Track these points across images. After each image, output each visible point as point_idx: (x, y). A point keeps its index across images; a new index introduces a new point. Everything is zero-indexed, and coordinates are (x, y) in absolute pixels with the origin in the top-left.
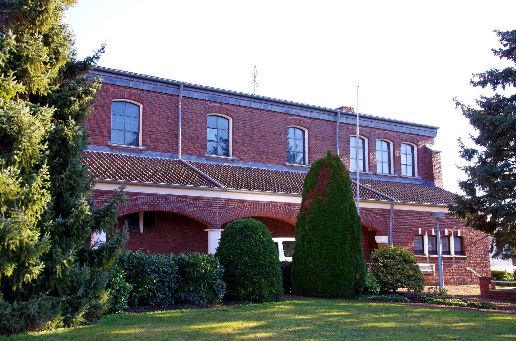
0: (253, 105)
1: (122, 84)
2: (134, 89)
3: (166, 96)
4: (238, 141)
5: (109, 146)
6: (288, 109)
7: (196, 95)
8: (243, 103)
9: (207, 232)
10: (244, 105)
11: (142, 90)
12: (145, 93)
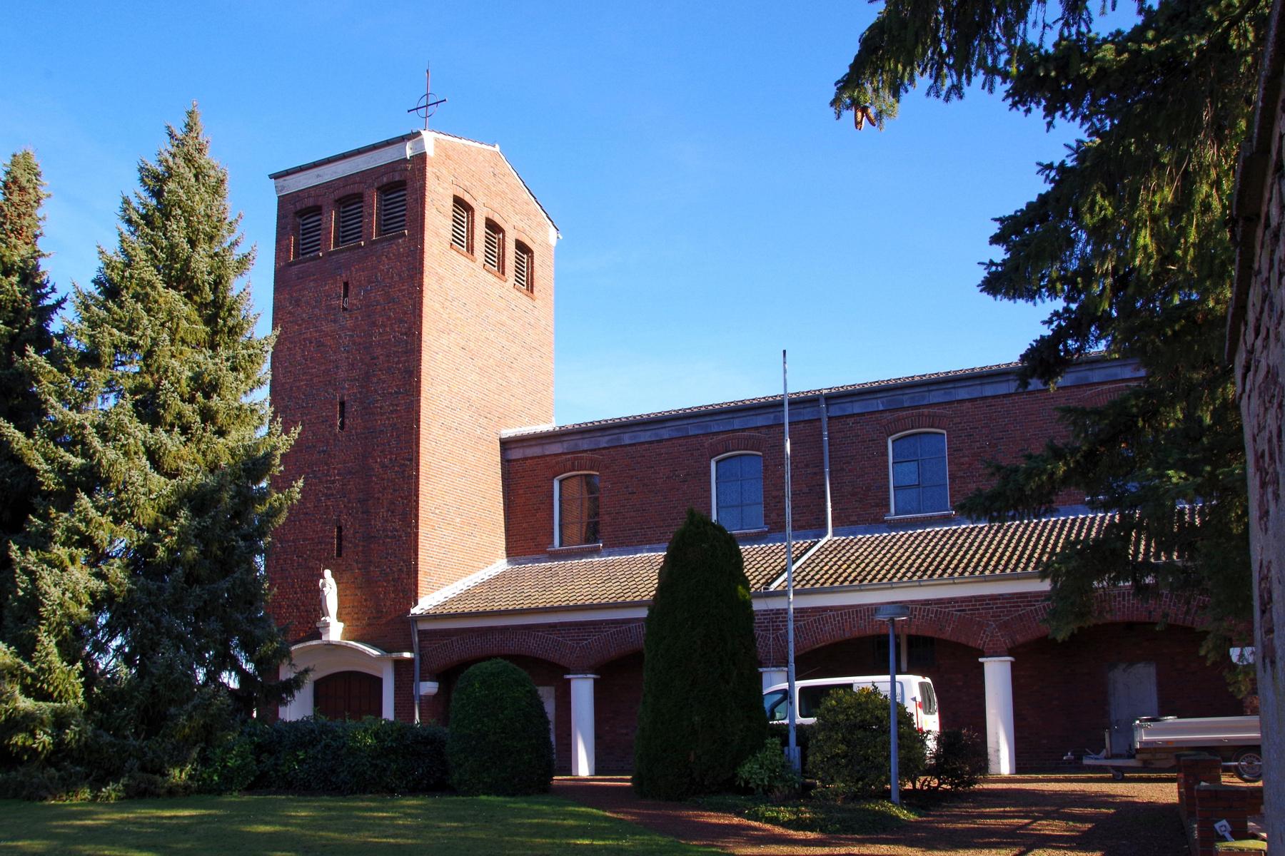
0: (989, 391)
1: (722, 429)
2: (744, 430)
3: (801, 426)
4: (961, 474)
5: (885, 521)
6: (1079, 374)
7: (857, 408)
8: (963, 394)
9: (569, 680)
10: (765, 423)
11: (757, 428)
12: (968, 404)
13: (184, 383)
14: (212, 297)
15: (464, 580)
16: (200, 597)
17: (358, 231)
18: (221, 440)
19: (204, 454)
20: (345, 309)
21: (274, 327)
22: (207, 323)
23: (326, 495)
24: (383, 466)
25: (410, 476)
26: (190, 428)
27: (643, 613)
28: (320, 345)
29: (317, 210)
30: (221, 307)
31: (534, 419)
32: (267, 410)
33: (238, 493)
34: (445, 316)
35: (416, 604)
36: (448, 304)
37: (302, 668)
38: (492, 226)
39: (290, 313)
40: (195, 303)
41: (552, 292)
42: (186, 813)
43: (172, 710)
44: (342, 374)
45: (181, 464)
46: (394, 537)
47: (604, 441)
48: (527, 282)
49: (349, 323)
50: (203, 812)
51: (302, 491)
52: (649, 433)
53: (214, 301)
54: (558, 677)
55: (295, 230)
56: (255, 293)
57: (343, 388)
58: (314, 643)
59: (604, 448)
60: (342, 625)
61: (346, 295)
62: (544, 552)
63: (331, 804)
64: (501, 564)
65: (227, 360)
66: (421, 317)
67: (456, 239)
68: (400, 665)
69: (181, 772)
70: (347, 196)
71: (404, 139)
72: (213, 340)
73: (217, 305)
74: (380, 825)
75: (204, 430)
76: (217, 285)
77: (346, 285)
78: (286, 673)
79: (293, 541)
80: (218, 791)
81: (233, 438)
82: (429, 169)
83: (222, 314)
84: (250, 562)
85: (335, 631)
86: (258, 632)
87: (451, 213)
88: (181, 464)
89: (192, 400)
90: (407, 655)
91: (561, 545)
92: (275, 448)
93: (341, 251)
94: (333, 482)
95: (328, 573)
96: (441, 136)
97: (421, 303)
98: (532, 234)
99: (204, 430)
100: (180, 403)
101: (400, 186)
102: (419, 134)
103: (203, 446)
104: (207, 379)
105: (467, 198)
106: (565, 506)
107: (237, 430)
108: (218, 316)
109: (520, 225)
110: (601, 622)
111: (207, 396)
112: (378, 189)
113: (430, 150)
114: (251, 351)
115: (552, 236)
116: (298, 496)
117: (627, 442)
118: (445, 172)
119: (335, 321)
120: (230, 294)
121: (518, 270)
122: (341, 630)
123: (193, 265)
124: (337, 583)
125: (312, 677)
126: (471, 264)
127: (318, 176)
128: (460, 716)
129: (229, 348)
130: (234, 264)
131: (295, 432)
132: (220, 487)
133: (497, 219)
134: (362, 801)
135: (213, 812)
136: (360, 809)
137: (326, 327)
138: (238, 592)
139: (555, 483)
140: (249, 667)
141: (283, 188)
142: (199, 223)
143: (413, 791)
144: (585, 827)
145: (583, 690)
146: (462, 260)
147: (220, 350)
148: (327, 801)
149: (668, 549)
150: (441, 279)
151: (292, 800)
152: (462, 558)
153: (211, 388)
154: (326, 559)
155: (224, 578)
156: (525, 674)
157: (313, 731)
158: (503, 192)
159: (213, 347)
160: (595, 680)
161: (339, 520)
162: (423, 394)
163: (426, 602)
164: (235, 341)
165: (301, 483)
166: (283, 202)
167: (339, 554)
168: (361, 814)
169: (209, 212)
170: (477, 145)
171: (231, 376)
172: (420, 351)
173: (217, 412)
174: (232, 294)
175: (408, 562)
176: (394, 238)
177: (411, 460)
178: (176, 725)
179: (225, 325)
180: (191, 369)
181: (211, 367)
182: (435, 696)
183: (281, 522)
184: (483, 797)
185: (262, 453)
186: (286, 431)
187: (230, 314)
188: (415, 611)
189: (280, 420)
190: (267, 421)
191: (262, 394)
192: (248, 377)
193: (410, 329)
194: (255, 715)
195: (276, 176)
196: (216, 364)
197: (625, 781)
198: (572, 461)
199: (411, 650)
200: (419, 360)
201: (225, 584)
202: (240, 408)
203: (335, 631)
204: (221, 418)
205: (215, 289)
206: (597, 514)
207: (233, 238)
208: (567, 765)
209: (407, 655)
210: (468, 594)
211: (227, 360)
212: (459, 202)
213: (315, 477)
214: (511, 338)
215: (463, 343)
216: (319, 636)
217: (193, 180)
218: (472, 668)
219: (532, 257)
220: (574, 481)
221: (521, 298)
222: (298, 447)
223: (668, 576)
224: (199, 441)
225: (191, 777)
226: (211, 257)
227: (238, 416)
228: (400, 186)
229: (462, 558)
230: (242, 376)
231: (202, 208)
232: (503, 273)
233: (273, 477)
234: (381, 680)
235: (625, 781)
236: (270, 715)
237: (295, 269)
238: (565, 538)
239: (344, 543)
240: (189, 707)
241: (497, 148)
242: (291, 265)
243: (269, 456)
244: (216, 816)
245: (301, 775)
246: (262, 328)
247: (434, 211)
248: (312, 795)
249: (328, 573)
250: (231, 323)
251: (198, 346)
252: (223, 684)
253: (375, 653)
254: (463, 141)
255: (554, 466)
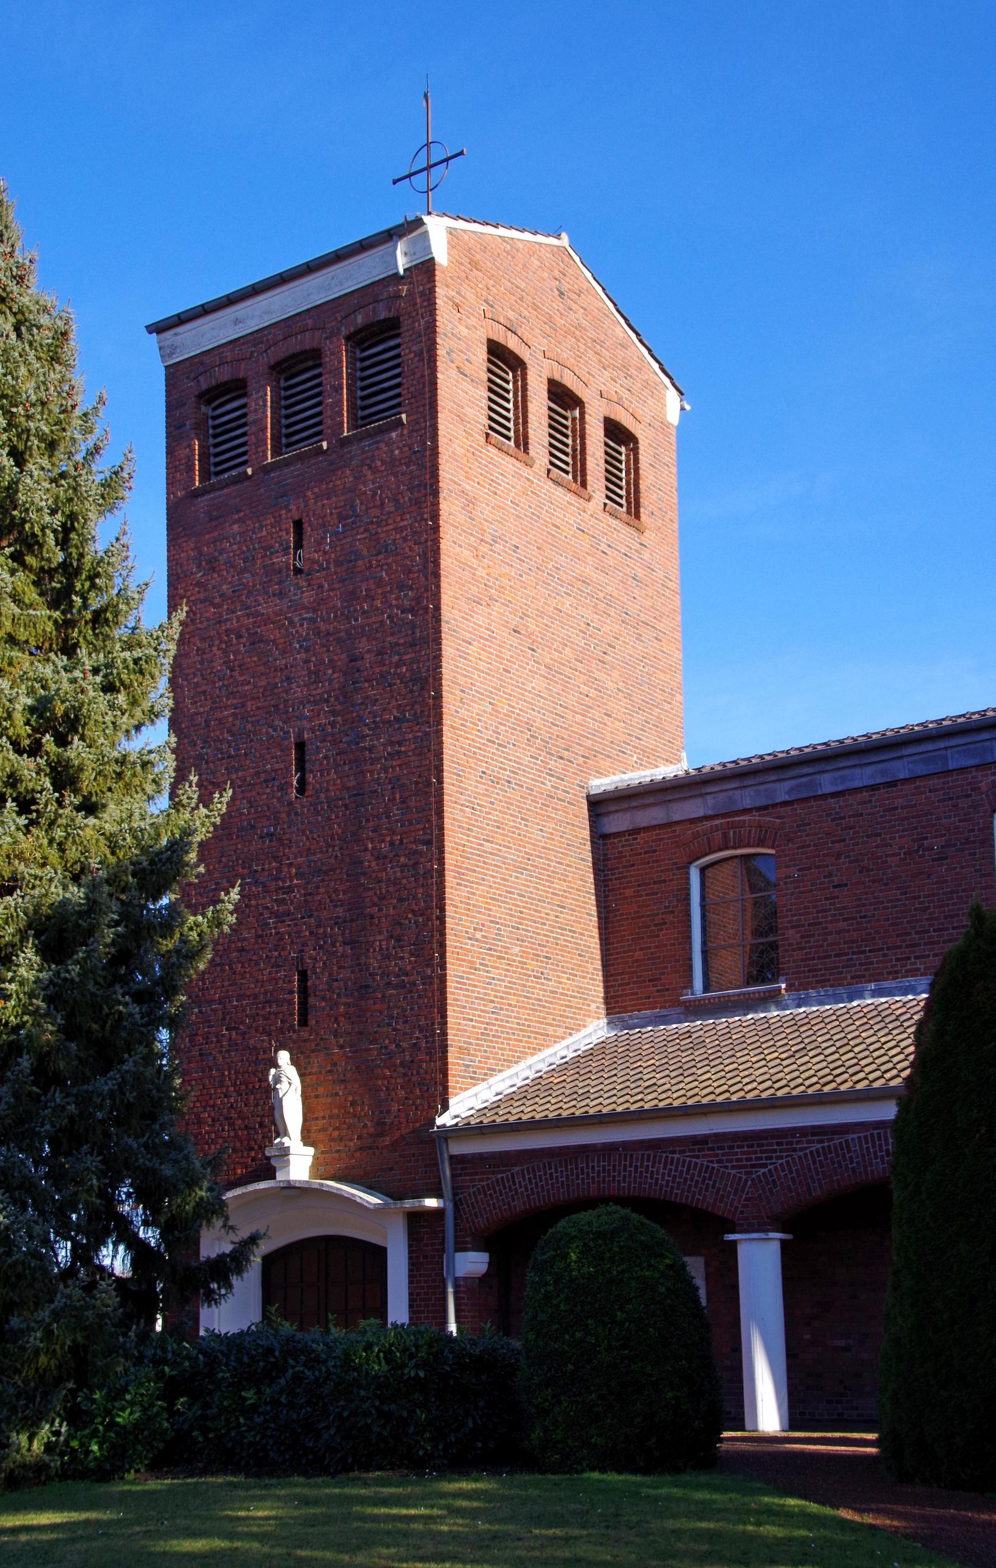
9: (734, 1243)
13: (19, 718)
14: (60, 557)
15: (531, 1060)
16: (63, 1108)
17: (317, 415)
18: (91, 821)
19: (62, 848)
20: (298, 571)
21: (173, 607)
22: (53, 605)
23: (276, 915)
24: (379, 857)
25: (428, 873)
26: (34, 801)
27: (888, 1111)
28: (256, 640)
29: (238, 387)
30: (78, 572)
31: (649, 757)
32: (166, 766)
33: (125, 917)
34: (481, 572)
35: (446, 1107)
36: (484, 549)
37: (244, 1234)
38: (561, 396)
39: (199, 584)
40: (31, 569)
41: (673, 515)
42: (45, 1518)
43: (15, 1322)
44: (298, 692)
45: (21, 867)
46: (402, 985)
47: (782, 791)
48: (627, 498)
49: (308, 597)
50: (75, 1516)
51: (237, 909)
52: (869, 770)
53: (64, 565)
54: (710, 1233)
55: (200, 427)
56: (135, 542)
57: (301, 718)
58: (262, 1185)
59: (785, 803)
60: (311, 1151)
61: (299, 545)
62: (676, 1003)
63: (306, 1491)
64: (596, 1029)
65: (96, 671)
66: (437, 576)
67: (496, 426)
68: (417, 1219)
69: (31, 1439)
70: (292, 359)
71: (391, 235)
72: (66, 640)
73: (69, 570)
74: (406, 1534)
75: (60, 803)
76: (65, 536)
77: (298, 525)
78: (214, 1244)
79: (220, 1001)
80: (105, 1472)
81: (110, 818)
82: (441, 292)
83: (78, 587)
84: (149, 1040)
85: (300, 1164)
86: (167, 1170)
87: (485, 376)
88: (21, 867)
89: (35, 750)
90: (431, 1203)
91: (706, 988)
92: (187, 832)
93: (287, 463)
94: (290, 890)
95: (284, 1057)
96: (461, 224)
97: (437, 551)
98: (635, 405)
99: (60, 803)
100: (12, 756)
101: (390, 327)
102: (419, 223)
103: (59, 834)
104: (60, 709)
105: (512, 343)
106: (712, 917)
107: (119, 803)
108: (71, 589)
109: (613, 389)
110: (793, 1131)
111: (62, 741)
112: (348, 338)
113: (440, 252)
114: (137, 653)
115: (672, 405)
116: (232, 919)
117: (828, 788)
118: (470, 296)
119: (281, 594)
120: (90, 548)
121: (611, 478)
122: (309, 1161)
123: (21, 497)
124: (301, 1075)
125: (265, 1247)
126: (525, 471)
127: (237, 322)
128: (542, 1317)
129: (96, 650)
130: (95, 490)
131: (222, 800)
132: (93, 906)
133: (569, 381)
134: (366, 1484)
135: (93, 1515)
136: (363, 1501)
137: (266, 607)
138: (131, 1097)
139: (704, 873)
140: (150, 1235)
141: (174, 349)
142: (29, 417)
143: (460, 1464)
144: (804, 1541)
145: (760, 1263)
146: (509, 464)
147: (82, 653)
148: (300, 1486)
149: (932, 988)
150: (470, 502)
151: (235, 1486)
152: (527, 1020)
153: (68, 726)
154: (281, 1031)
155: (104, 1072)
156: (661, 1233)
157: (270, 1351)
158: (579, 327)
159: (69, 649)
160: (784, 1244)
161: (301, 960)
162: (447, 720)
163: (462, 1105)
164: (107, 637)
165: (235, 894)
166: (174, 375)
167: (304, 1022)
168: (369, 1510)
169: (43, 395)
170: (527, 236)
171: (103, 700)
172: (438, 641)
173: (81, 769)
174: (97, 548)
175: (428, 1031)
176: (380, 431)
177: (428, 843)
178: (22, 1348)
179: (85, 606)
180: (31, 692)
181: (66, 686)
182: (483, 1279)
183: (202, 966)
184: (596, 1475)
185: (164, 841)
186: (205, 800)
187: (93, 586)
188: (445, 1120)
189: (194, 779)
190: (166, 785)
191: (158, 735)
192: (134, 702)
193: (418, 599)
194: (159, 1327)
195: (158, 328)
196: (73, 681)
197: (863, 1443)
198: (727, 829)
199: (439, 1195)
200: (438, 657)
201: (105, 1085)
202: (122, 761)
203: (300, 1164)
204: (87, 781)
205: (63, 543)
206: (772, 929)
207: (91, 441)
208: (733, 1402)
209: (431, 1203)
210: (538, 1086)
211: (96, 671)
212: (497, 351)
213: (256, 883)
214: (602, 606)
215: (514, 621)
216: (270, 1173)
217: (13, 336)
218: (562, 1223)
219: (635, 451)
220: (726, 868)
221: (616, 530)
222: (226, 829)
223: (935, 1039)
224: (52, 823)
225: (49, 1448)
226: (52, 481)
227: (119, 775)
228: (390, 327)
229: (527, 1020)
230: (122, 699)
231: (31, 385)
232: (584, 484)
233: (186, 892)
234: (385, 1249)
235: (863, 1443)
236: (184, 1326)
237: (203, 502)
238: (713, 977)
239: (311, 1000)
240: (45, 1314)
241: (565, 241)
242: (196, 494)
243: (177, 847)
244: (97, 1522)
245: (250, 1437)
246: (151, 610)
247: (454, 373)
248: (270, 1475)
249: (284, 1057)
250: (96, 602)
251: (40, 650)
252: (102, 1269)
253: (373, 1200)
254: (502, 231)
255: (687, 843)
